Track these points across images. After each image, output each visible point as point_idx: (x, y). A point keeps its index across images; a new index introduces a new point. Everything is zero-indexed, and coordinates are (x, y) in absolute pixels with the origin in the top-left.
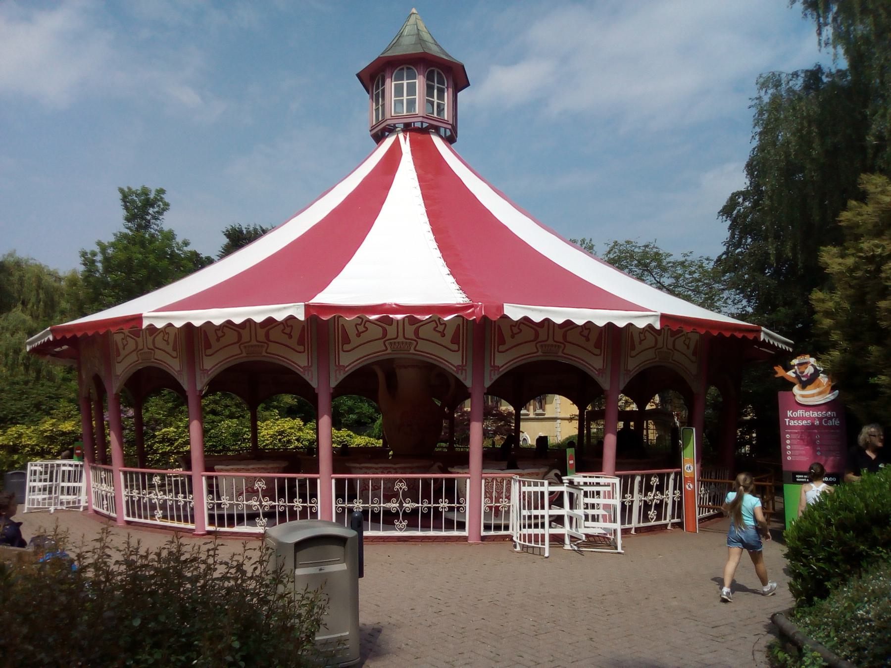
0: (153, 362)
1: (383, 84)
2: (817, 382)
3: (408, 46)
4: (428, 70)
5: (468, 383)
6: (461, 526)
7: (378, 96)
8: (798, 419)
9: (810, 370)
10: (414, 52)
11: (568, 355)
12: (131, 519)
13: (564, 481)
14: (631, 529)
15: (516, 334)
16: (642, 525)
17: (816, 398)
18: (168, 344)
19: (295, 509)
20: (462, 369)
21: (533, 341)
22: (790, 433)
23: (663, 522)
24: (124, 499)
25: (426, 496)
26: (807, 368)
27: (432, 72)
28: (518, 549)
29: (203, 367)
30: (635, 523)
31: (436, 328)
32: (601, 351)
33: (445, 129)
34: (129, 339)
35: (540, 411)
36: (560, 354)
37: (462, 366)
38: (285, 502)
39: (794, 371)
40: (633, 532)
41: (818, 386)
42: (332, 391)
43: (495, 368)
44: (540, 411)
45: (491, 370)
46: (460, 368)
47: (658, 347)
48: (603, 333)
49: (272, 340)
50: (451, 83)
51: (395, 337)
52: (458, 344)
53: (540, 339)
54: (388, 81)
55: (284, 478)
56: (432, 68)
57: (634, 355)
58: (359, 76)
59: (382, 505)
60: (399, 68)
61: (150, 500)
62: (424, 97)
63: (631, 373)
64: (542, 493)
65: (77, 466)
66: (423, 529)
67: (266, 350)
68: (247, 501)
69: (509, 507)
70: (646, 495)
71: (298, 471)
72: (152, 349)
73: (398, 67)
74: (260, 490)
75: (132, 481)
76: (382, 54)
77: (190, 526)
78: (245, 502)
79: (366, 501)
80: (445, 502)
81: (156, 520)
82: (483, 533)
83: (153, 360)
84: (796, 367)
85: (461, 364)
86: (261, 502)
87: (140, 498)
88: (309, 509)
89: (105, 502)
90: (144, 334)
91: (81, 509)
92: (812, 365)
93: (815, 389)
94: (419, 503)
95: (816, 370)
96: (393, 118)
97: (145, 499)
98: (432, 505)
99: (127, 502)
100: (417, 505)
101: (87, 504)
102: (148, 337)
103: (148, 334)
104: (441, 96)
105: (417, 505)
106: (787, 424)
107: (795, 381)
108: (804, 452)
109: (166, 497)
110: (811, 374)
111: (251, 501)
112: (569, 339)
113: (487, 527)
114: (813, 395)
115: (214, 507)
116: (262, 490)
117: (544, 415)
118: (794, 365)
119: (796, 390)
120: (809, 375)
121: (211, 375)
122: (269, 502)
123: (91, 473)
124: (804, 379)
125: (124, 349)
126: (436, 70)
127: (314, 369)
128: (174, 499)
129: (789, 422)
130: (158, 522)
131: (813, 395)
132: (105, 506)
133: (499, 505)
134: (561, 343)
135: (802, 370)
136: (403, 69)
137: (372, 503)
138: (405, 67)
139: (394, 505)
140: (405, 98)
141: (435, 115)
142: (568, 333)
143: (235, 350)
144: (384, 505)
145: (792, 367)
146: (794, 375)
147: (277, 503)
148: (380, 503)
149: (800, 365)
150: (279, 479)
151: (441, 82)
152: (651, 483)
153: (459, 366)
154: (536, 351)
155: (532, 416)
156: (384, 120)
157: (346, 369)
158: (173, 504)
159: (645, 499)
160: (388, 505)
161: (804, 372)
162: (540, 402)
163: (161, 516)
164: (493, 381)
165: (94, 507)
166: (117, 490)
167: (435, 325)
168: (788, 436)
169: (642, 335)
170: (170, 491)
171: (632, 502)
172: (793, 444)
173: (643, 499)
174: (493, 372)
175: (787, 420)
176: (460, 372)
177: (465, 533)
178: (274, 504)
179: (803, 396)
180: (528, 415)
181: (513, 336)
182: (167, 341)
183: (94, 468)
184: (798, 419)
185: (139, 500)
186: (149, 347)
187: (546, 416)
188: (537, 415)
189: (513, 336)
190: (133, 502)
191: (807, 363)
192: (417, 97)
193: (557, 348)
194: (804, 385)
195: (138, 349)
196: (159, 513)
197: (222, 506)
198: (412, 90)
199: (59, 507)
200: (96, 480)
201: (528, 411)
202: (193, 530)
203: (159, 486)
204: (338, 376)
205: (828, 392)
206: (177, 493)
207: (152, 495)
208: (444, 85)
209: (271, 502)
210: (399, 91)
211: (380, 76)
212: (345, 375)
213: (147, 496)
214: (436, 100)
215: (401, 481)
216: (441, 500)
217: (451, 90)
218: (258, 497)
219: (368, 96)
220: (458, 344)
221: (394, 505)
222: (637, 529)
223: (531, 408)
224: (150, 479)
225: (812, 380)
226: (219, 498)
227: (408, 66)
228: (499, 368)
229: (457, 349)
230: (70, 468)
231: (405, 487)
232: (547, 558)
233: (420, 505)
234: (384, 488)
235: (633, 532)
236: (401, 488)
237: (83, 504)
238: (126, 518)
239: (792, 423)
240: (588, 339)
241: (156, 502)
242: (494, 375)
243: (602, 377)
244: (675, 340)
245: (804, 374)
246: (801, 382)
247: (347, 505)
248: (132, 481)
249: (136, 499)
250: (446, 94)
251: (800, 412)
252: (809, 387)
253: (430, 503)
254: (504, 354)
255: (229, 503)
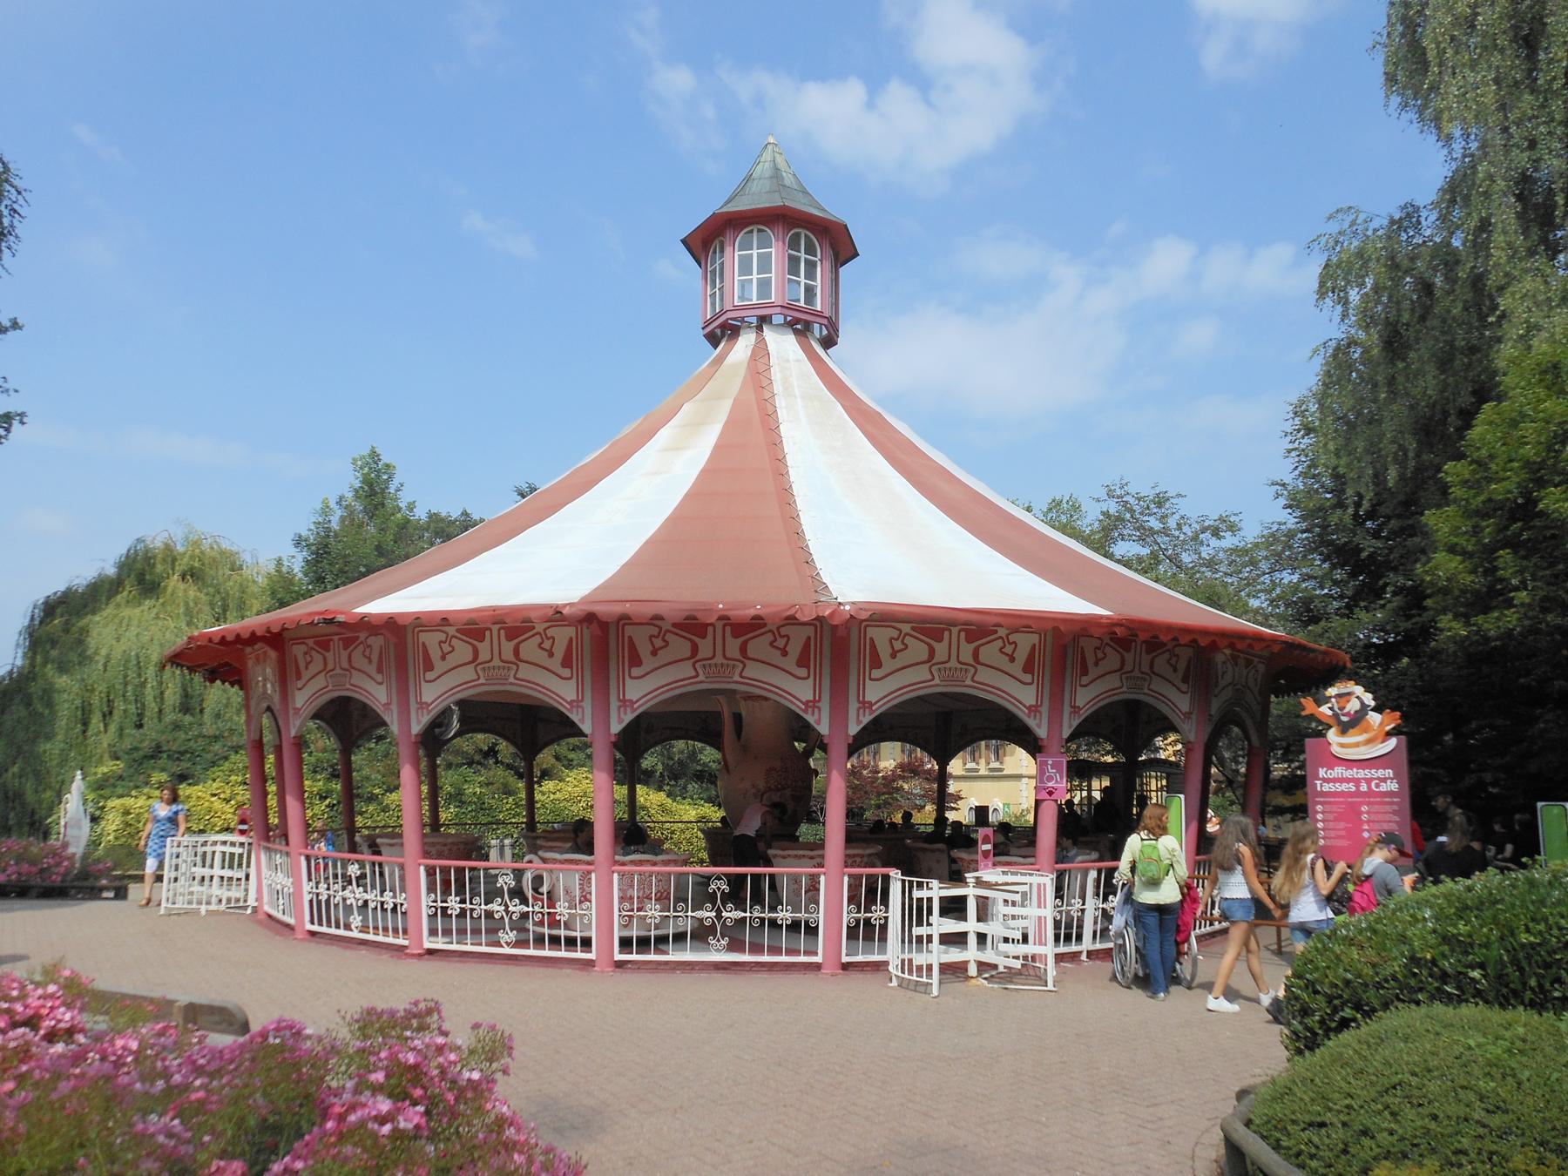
0: (348, 689)
1: (722, 251)
2: (1363, 724)
3: (759, 198)
4: (792, 232)
5: (824, 729)
6: (587, 943)
7: (713, 276)
8: (1334, 780)
9: (1353, 706)
10: (767, 205)
11: (522, 680)
12: (316, 928)
13: (968, 880)
14: (1081, 952)
15: (448, 653)
16: (1098, 946)
17: (1362, 749)
18: (370, 662)
19: (558, 918)
20: (814, 707)
21: (469, 663)
22: (1322, 803)
23: (1074, 948)
24: (307, 898)
25: (758, 899)
26: (1348, 702)
27: (797, 237)
28: (895, 983)
29: (864, 697)
30: (1087, 944)
31: (654, 636)
32: (1033, 675)
33: (821, 324)
34: (1108, 650)
35: (996, 765)
36: (512, 680)
37: (814, 701)
38: (543, 907)
39: (1329, 705)
40: (1084, 957)
41: (1365, 731)
42: (613, 739)
43: (865, 705)
44: (996, 765)
45: (620, 707)
46: (811, 704)
47: (328, 669)
48: (1037, 647)
49: (525, 659)
50: (829, 252)
51: (710, 655)
52: (808, 667)
53: (699, 656)
54: (728, 250)
55: (861, 876)
56: (797, 230)
57: (432, 679)
58: (684, 241)
59: (690, 914)
60: (745, 230)
61: (344, 900)
62: (784, 275)
63: (1082, 712)
64: (930, 900)
65: (242, 844)
66: (552, 946)
67: (741, 672)
68: (486, 905)
69: (886, 918)
70: (1105, 899)
71: (469, 858)
72: (1147, 674)
73: (745, 227)
74: (506, 889)
75: (317, 869)
76: (727, 203)
77: (401, 941)
78: (483, 907)
79: (797, 909)
80: (787, 911)
81: (351, 930)
82: (619, 957)
83: (348, 686)
84: (1333, 700)
85: (575, 698)
86: (507, 906)
87: (329, 896)
88: (468, 912)
89: (281, 901)
90: (1139, 648)
91: (249, 911)
92: (1358, 697)
93: (1362, 734)
94: (746, 912)
95: (1364, 706)
96: (737, 308)
97: (337, 899)
98: (862, 915)
99: (311, 901)
100: (743, 914)
101: (256, 904)
102: (342, 651)
103: (1144, 648)
104: (810, 275)
105: (743, 914)
106: (1319, 789)
107: (1331, 722)
108: (1343, 833)
109: (367, 897)
110: (1356, 712)
111: (491, 905)
112: (523, 655)
113: (626, 943)
114: (1357, 745)
115: (436, 913)
116: (509, 889)
117: (1001, 770)
118: (1330, 697)
119: (1332, 735)
120: (1352, 712)
121: (434, 712)
122: (518, 907)
123: (263, 857)
124: (1345, 719)
125: (307, 668)
126: (803, 232)
127: (587, 705)
128: (379, 898)
129: (1321, 786)
130: (355, 934)
131: (1357, 745)
132: (281, 907)
133: (870, 915)
134: (511, 663)
135: (1341, 705)
136: (752, 231)
137: (675, 911)
138: (755, 228)
139: (709, 914)
140: (755, 276)
141: (802, 304)
142: (982, 649)
143: (922, 673)
144: (693, 914)
145: (1327, 700)
146: (1330, 713)
147: (530, 909)
148: (687, 911)
149: (1339, 696)
150: (869, 876)
151: (810, 250)
152: (1114, 881)
153: (808, 701)
154: (930, 677)
155: (983, 772)
156: (723, 312)
157: (635, 706)
158: (376, 908)
159: (1105, 906)
160: (699, 914)
161: (1344, 708)
162: (973, 753)
163: (360, 924)
164: (862, 726)
165: (267, 908)
166: (297, 885)
167: (896, 636)
168: (1319, 808)
169: (308, 656)
170: (373, 887)
171: (1083, 911)
172: (1327, 821)
173: (1101, 906)
174: (861, 711)
175: (1318, 782)
176: (810, 710)
177: (818, 959)
178: (526, 909)
179: (1342, 745)
180: (977, 770)
181: (894, 655)
182: (369, 658)
183: (268, 849)
184: (1334, 780)
185: (328, 901)
186: (1143, 669)
187: (1004, 773)
188: (991, 770)
189: (894, 655)
190: (319, 902)
191: (1349, 694)
192: (773, 275)
193: (963, 672)
194: (1344, 729)
195: (1124, 670)
196: (356, 920)
197: (449, 912)
198: (764, 265)
199: (213, 907)
200: (269, 868)
201: (977, 764)
202: (406, 947)
203: (358, 879)
204: (861, 718)
205: (1380, 740)
206: (383, 891)
207: (347, 893)
208: (816, 256)
209: (522, 906)
210: (746, 268)
211: (717, 242)
212: (873, 716)
213: (340, 893)
214: (802, 279)
215: (719, 878)
216: (780, 907)
217: (827, 264)
218: (714, 903)
219: (699, 271)
220: (808, 667)
221: (709, 914)
222: (1090, 953)
223: (983, 761)
224: (344, 867)
225: (1357, 720)
226: (552, 905)
227: (760, 227)
228: (632, 703)
229: (569, 675)
230: (233, 850)
231: (725, 887)
232: (935, 997)
233: (748, 914)
234: (455, 881)
235: (1084, 957)
236: (719, 889)
237: (252, 902)
238: (309, 927)
239: (1327, 787)
240: (551, 655)
241: (352, 904)
242: (625, 713)
243: (1035, 718)
244: (1153, 659)
245: (1346, 711)
246: (1340, 722)
247: (802, 915)
248: (317, 869)
249: (323, 898)
250: (819, 269)
251: (1338, 771)
252: (1351, 731)
253: (859, 912)
254: (641, 680)
255: (569, 914)
